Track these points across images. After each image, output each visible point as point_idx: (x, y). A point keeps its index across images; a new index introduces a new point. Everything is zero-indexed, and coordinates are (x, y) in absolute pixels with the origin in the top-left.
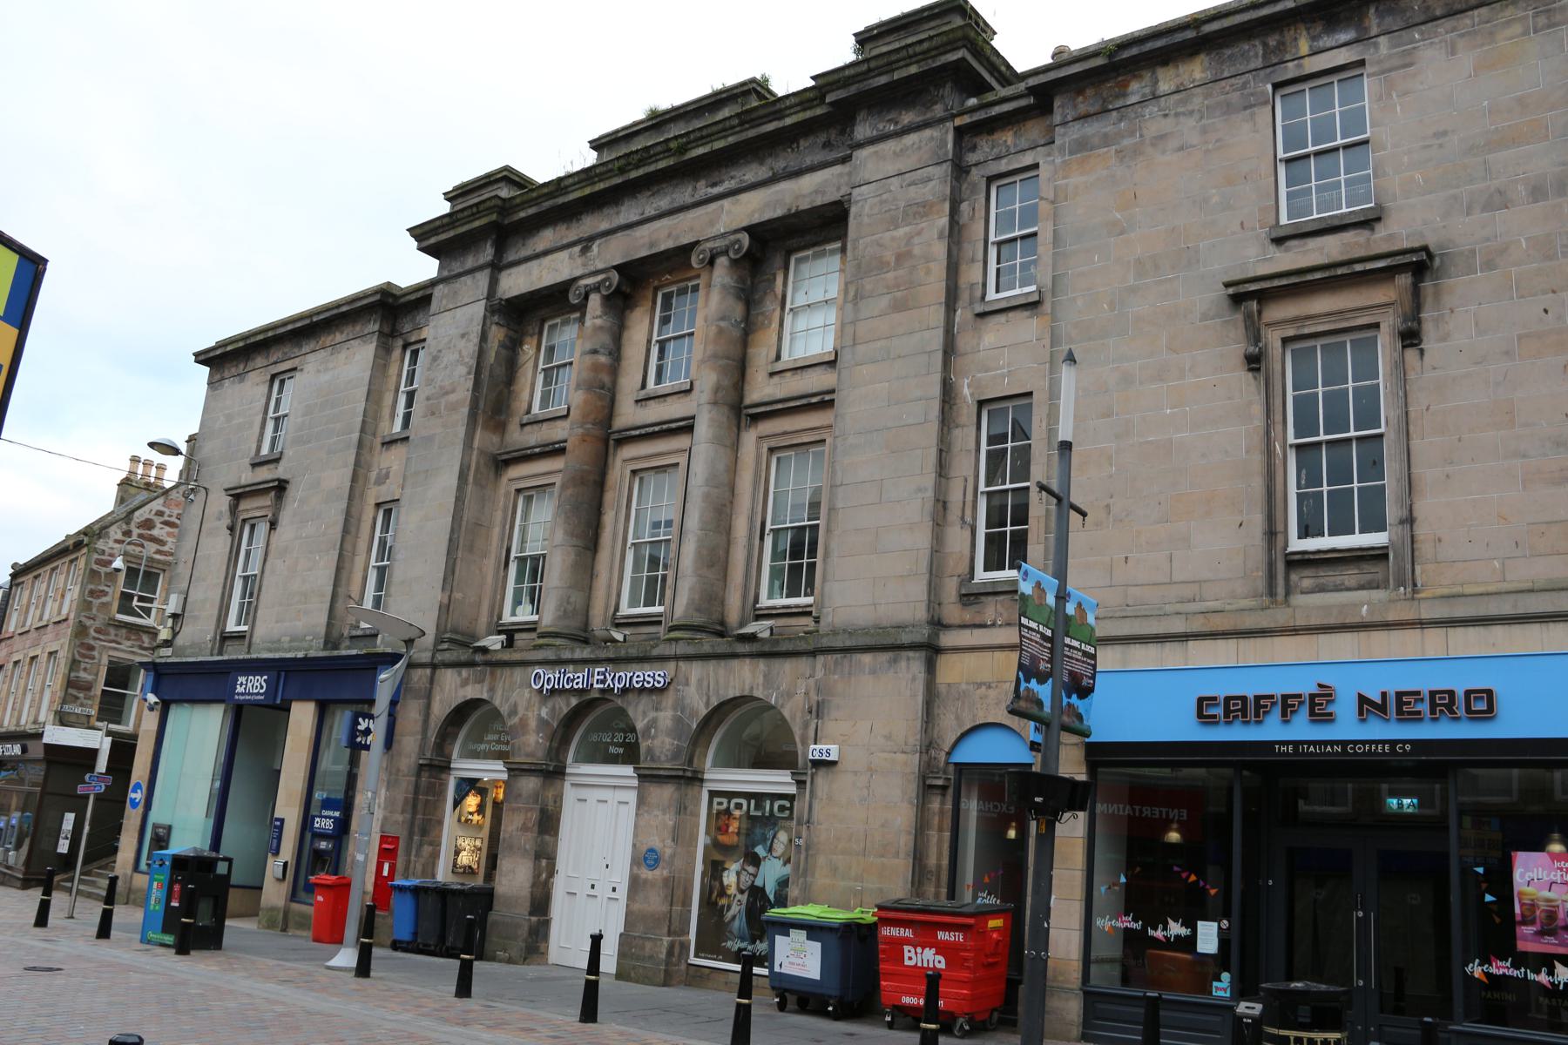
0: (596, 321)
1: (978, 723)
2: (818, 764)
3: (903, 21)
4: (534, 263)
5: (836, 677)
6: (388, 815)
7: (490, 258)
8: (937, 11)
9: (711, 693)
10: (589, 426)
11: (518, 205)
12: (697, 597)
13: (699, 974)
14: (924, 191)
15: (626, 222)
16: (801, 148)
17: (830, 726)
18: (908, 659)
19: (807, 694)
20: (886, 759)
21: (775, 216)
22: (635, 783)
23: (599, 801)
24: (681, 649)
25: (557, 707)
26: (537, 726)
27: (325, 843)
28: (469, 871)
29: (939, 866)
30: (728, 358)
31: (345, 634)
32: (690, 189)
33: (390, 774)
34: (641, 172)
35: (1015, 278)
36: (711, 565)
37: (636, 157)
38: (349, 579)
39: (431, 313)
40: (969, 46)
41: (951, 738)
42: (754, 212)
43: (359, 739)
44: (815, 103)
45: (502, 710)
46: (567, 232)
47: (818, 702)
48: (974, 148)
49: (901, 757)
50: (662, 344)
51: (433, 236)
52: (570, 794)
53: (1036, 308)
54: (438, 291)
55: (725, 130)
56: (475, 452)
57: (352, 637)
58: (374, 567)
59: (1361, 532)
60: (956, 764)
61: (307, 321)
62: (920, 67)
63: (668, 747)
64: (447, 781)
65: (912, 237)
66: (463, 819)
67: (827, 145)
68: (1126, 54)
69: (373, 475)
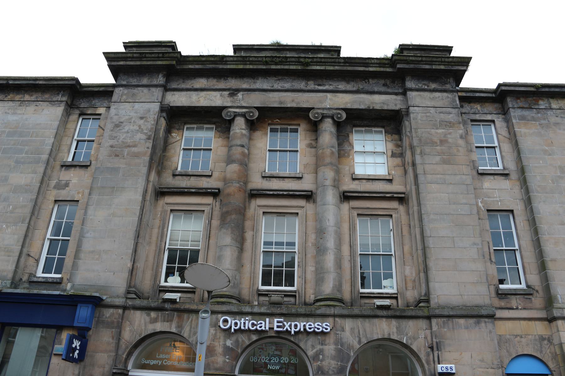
1: (519, 354)
5: (445, 330)
9: (361, 336)
10: (242, 183)
11: (189, 61)
17: (445, 355)
18: (485, 322)
19: (426, 338)
20: (483, 372)
21: (361, 108)
25: (240, 340)
34: (279, 67)
37: (278, 60)
42: (347, 103)
44: (387, 66)
46: (217, 83)
47: (437, 343)
53: (507, 176)
59: (167, 266)
61: (5, 82)
62: (270, 67)
63: (334, 366)
65: (446, 134)
67: (385, 85)
68: (543, 90)
69: (53, 183)
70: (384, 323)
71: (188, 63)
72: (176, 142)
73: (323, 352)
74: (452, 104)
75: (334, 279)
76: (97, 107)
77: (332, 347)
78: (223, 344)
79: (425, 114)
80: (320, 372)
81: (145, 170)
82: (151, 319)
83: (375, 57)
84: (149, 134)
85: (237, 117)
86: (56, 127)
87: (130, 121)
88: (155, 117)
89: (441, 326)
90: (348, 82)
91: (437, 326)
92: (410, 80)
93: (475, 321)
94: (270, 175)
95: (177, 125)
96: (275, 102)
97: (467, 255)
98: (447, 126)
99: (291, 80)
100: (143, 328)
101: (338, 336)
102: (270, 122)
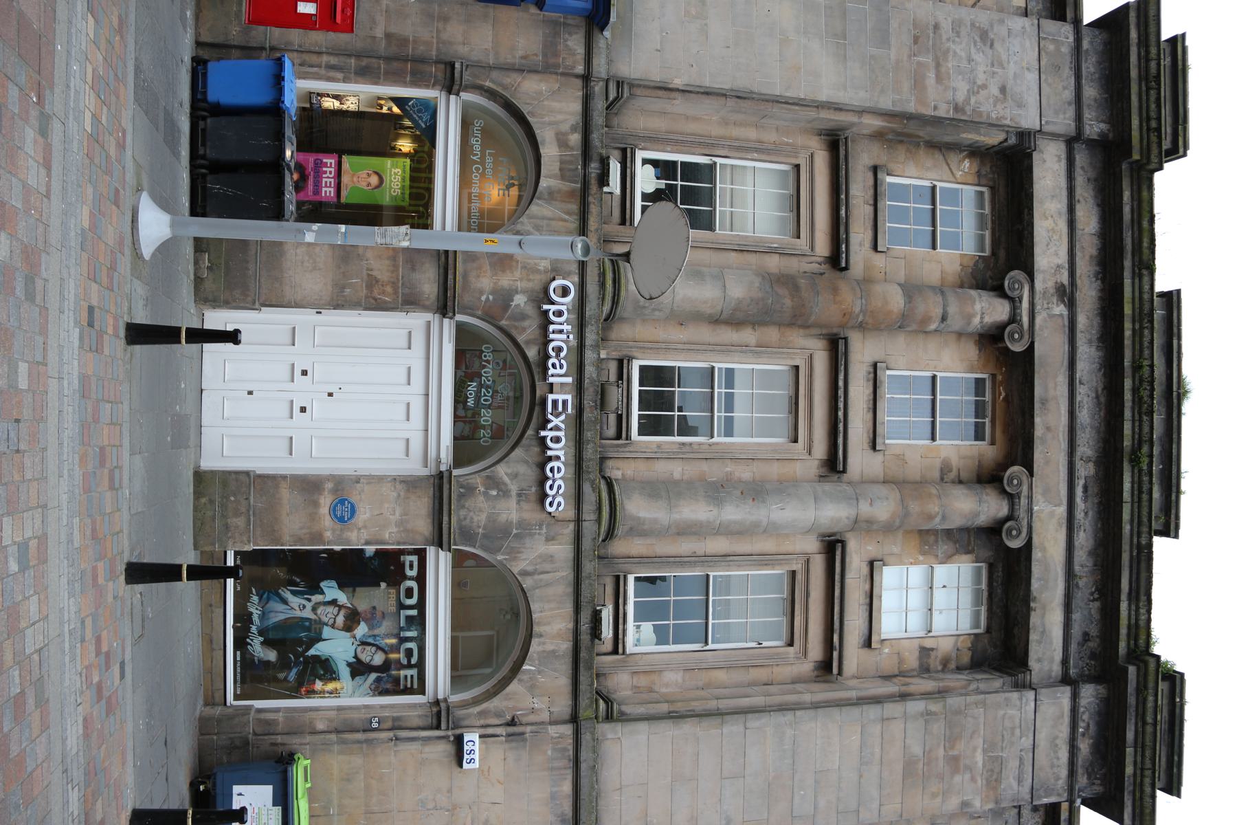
0: (979, 317)
2: (459, 741)
3: (1177, 733)
5: (549, 753)
8: (1175, 770)
9: (536, 577)
17: (499, 750)
19: (533, 711)
21: (1033, 581)
23: (409, 368)
25: (526, 323)
34: (1128, 396)
37: (1145, 394)
39: (1044, 22)
42: (1044, 550)
44: (1132, 642)
46: (1087, 257)
51: (1139, 38)
52: (417, 320)
55: (1140, 523)
63: (476, 519)
65: (971, 772)
66: (382, 102)
67: (1086, 637)
70: (564, 624)
72: (950, 169)
73: (504, 496)
75: (655, 520)
77: (514, 516)
78: (517, 287)
80: (462, 490)
81: (886, 103)
82: (565, 134)
87: (995, 63)
88: (1006, 119)
91: (557, 735)
95: (988, 170)
98: (989, 773)
101: (536, 529)
102: (1000, 378)
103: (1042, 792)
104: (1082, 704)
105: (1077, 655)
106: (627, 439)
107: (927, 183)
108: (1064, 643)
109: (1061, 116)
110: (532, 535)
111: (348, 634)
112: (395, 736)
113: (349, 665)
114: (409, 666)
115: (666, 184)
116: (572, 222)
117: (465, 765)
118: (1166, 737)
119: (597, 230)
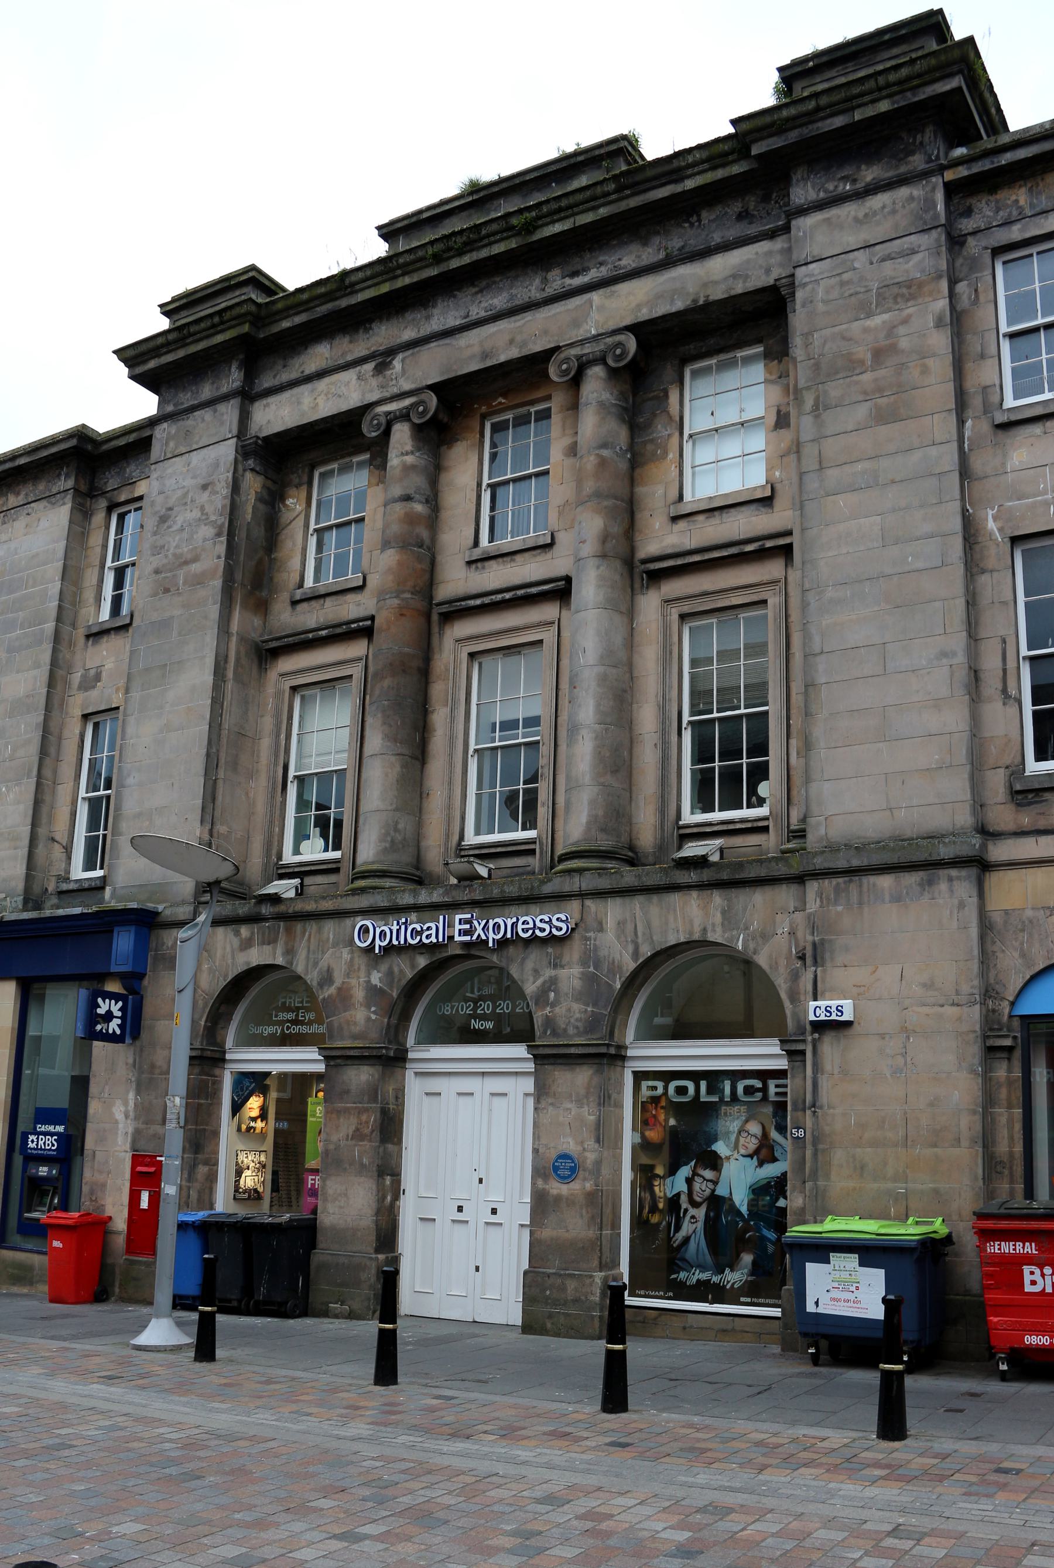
2: (820, 1027)
4: (304, 390)
5: (840, 908)
6: (141, 1126)
7: (237, 384)
9: (640, 940)
10: (408, 595)
12: (601, 813)
13: (640, 1318)
14: (906, 266)
15: (442, 328)
16: (705, 221)
17: (835, 975)
18: (950, 879)
19: (792, 933)
21: (674, 310)
22: (530, 1066)
23: (459, 1094)
24: (586, 882)
25: (396, 969)
26: (366, 997)
27: (45, 1169)
28: (254, 1195)
29: (1011, 1154)
30: (616, 498)
31: (50, 889)
32: (537, 281)
33: (141, 1071)
34: (466, 259)
35: (1042, 379)
36: (615, 771)
37: (460, 240)
38: (51, 817)
40: (966, 72)
41: (1015, 983)
42: (639, 307)
43: (99, 1027)
44: (730, 158)
45: (308, 978)
46: (351, 346)
47: (814, 944)
48: (968, 212)
49: (950, 1011)
50: (493, 487)
52: (414, 1088)
54: (160, 432)
55: (594, 198)
56: (234, 639)
57: (61, 893)
58: (84, 799)
60: (1023, 1017)
62: (893, 103)
63: (578, 1015)
64: (222, 1077)
65: (895, 327)
66: (244, 1127)
67: (743, 216)
69: (76, 678)
70: (693, 902)
71: (278, 317)
72: (294, 519)
73: (555, 984)
74: (921, 218)
75: (592, 803)
76: (135, 482)
77: (576, 971)
78: (365, 981)
79: (838, 279)
80: (549, 1033)
81: (214, 611)
82: (241, 941)
83: (694, 145)
84: (219, 522)
85: (393, 424)
86: (61, 553)
87: (184, 501)
88: (228, 477)
89: (828, 899)
90: (645, 242)
91: (818, 900)
92: (803, 179)
93: (922, 879)
94: (483, 554)
95: (295, 475)
96: (472, 357)
97: (918, 691)
98: (899, 300)
99: (509, 281)
100: (230, 961)
101: (590, 945)
102: (484, 409)
103: (928, 217)
104: (815, 196)
105: (765, 221)
106: (535, 843)
107: (1005, 346)
108: (748, 244)
109: (225, 417)
110: (596, 948)
111: (726, 1165)
112: (810, 1108)
113: (761, 1164)
114: (765, 1089)
115: (315, 827)
116: (311, 928)
117: (847, 1017)
118: (864, 60)
119: (316, 901)
